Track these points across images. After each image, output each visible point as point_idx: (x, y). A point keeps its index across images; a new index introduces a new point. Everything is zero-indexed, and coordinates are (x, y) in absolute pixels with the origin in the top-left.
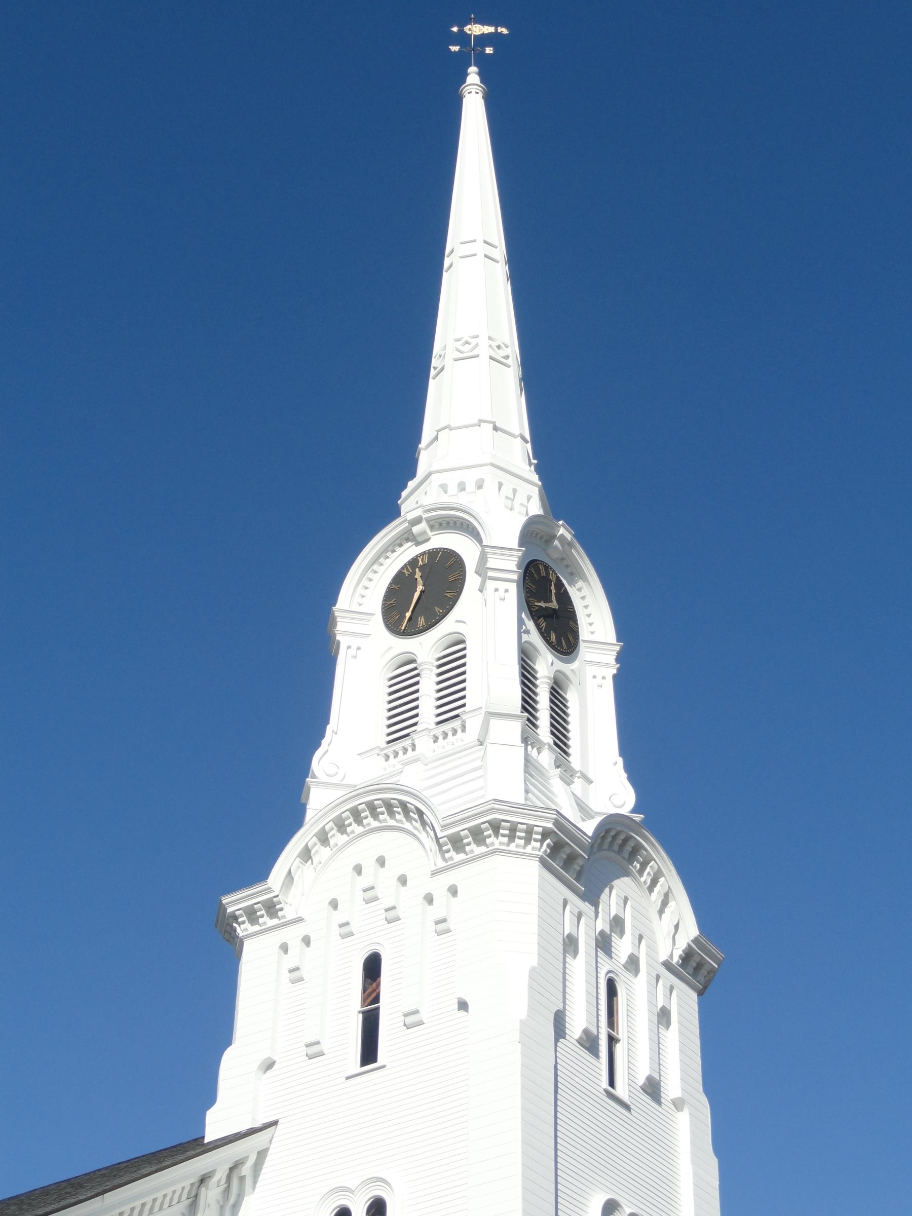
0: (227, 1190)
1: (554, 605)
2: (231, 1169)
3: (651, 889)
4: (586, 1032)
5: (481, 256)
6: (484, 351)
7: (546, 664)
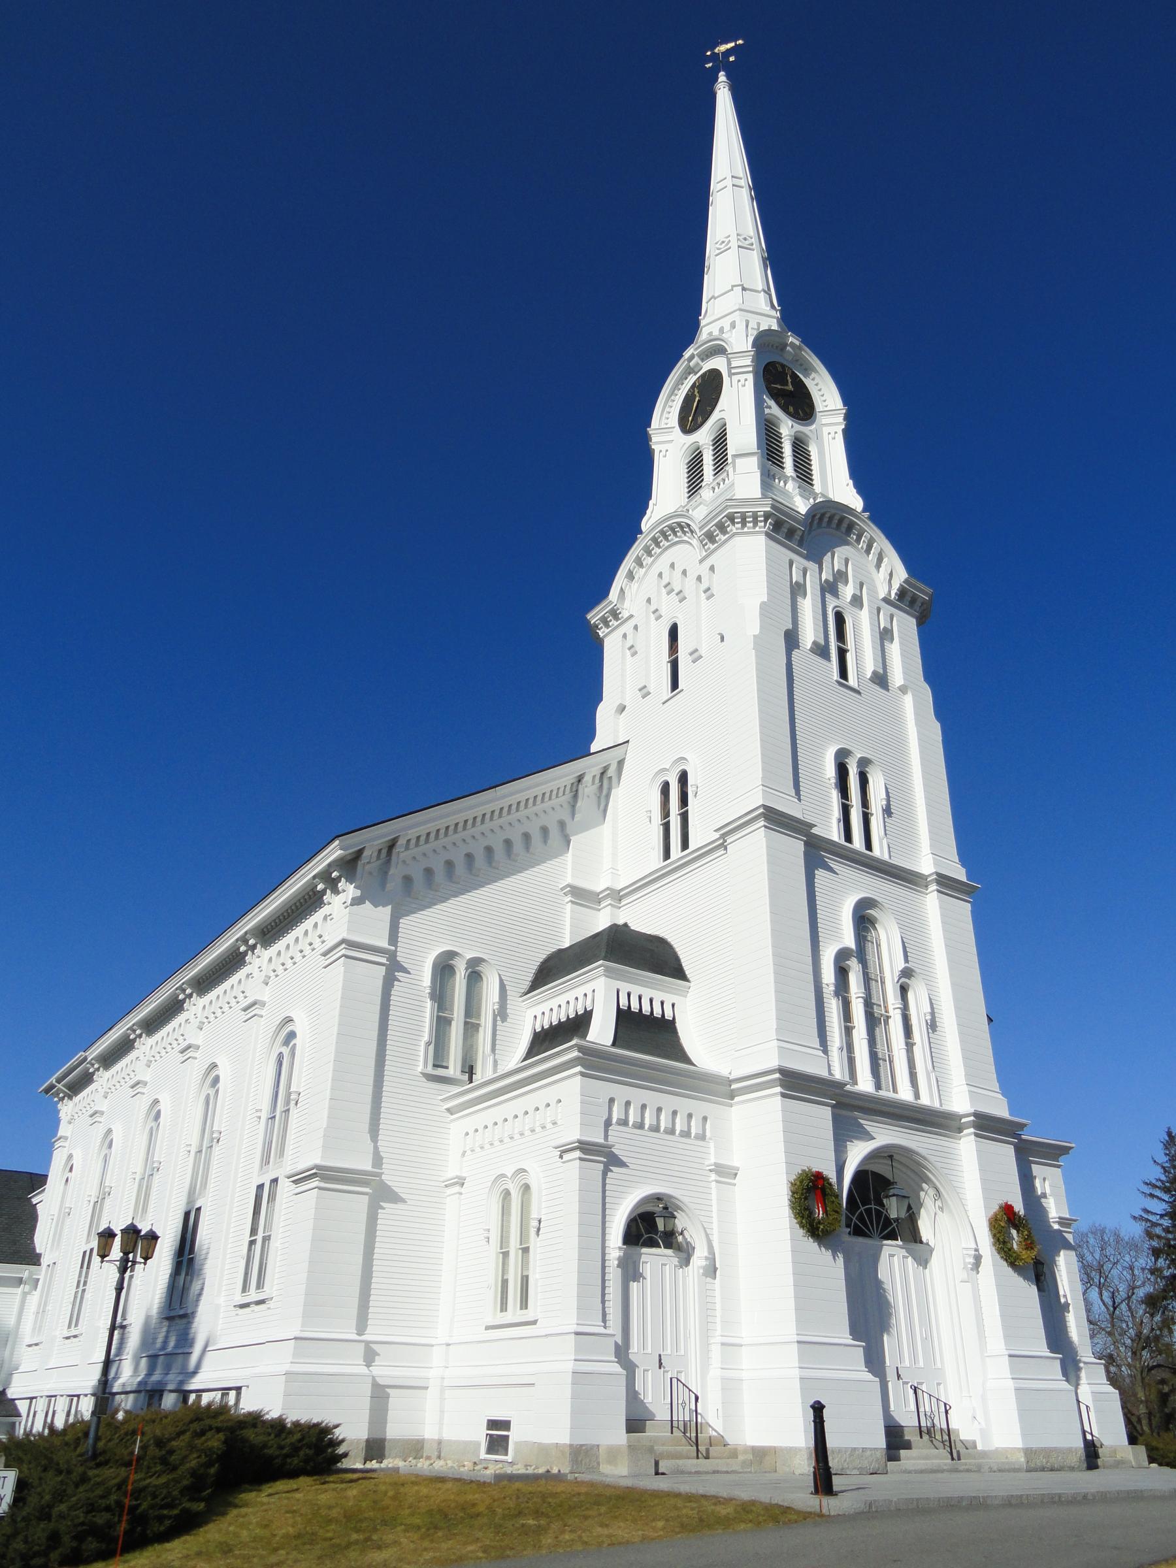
0: (601, 786)
1: (790, 387)
2: (602, 774)
3: (868, 551)
5: (730, 187)
6: (734, 244)
7: (787, 428)
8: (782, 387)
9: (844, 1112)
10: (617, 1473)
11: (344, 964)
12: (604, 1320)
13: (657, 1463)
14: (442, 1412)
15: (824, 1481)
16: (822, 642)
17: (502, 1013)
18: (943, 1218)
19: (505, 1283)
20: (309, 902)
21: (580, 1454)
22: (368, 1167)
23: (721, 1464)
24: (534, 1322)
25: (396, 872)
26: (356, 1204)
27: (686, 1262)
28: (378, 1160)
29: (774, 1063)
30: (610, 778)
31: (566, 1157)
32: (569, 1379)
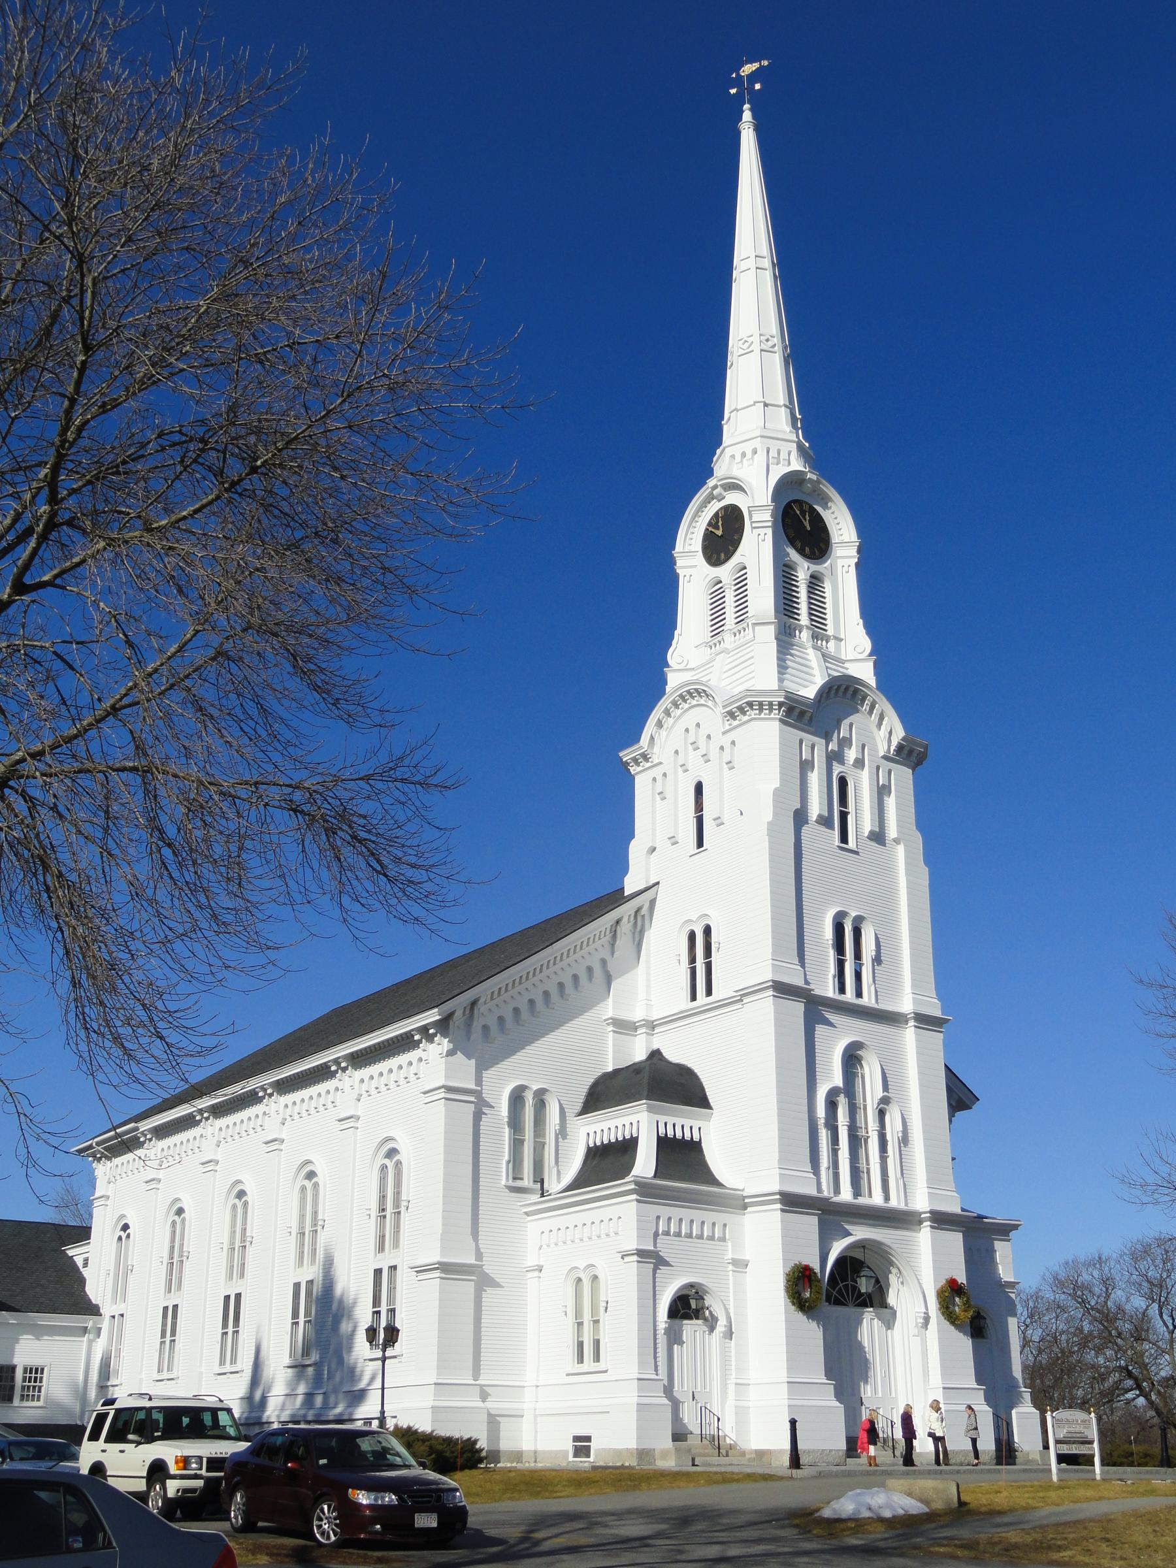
0: (635, 924)
2: (636, 912)
4: (820, 816)
6: (756, 347)
7: (803, 570)
8: (801, 530)
9: (827, 1217)
10: (669, 1463)
11: (445, 1105)
12: (656, 1370)
13: (693, 1460)
14: (536, 1432)
15: (795, 1461)
16: (826, 814)
17: (562, 1133)
18: (904, 1290)
19: (580, 1345)
20: (404, 1043)
21: (643, 1454)
22: (473, 1261)
23: (734, 1460)
24: (606, 1371)
25: (477, 1025)
26: (466, 1288)
27: (712, 1329)
28: (479, 1255)
29: (776, 1188)
30: (643, 916)
31: (627, 1259)
32: (635, 1408)
